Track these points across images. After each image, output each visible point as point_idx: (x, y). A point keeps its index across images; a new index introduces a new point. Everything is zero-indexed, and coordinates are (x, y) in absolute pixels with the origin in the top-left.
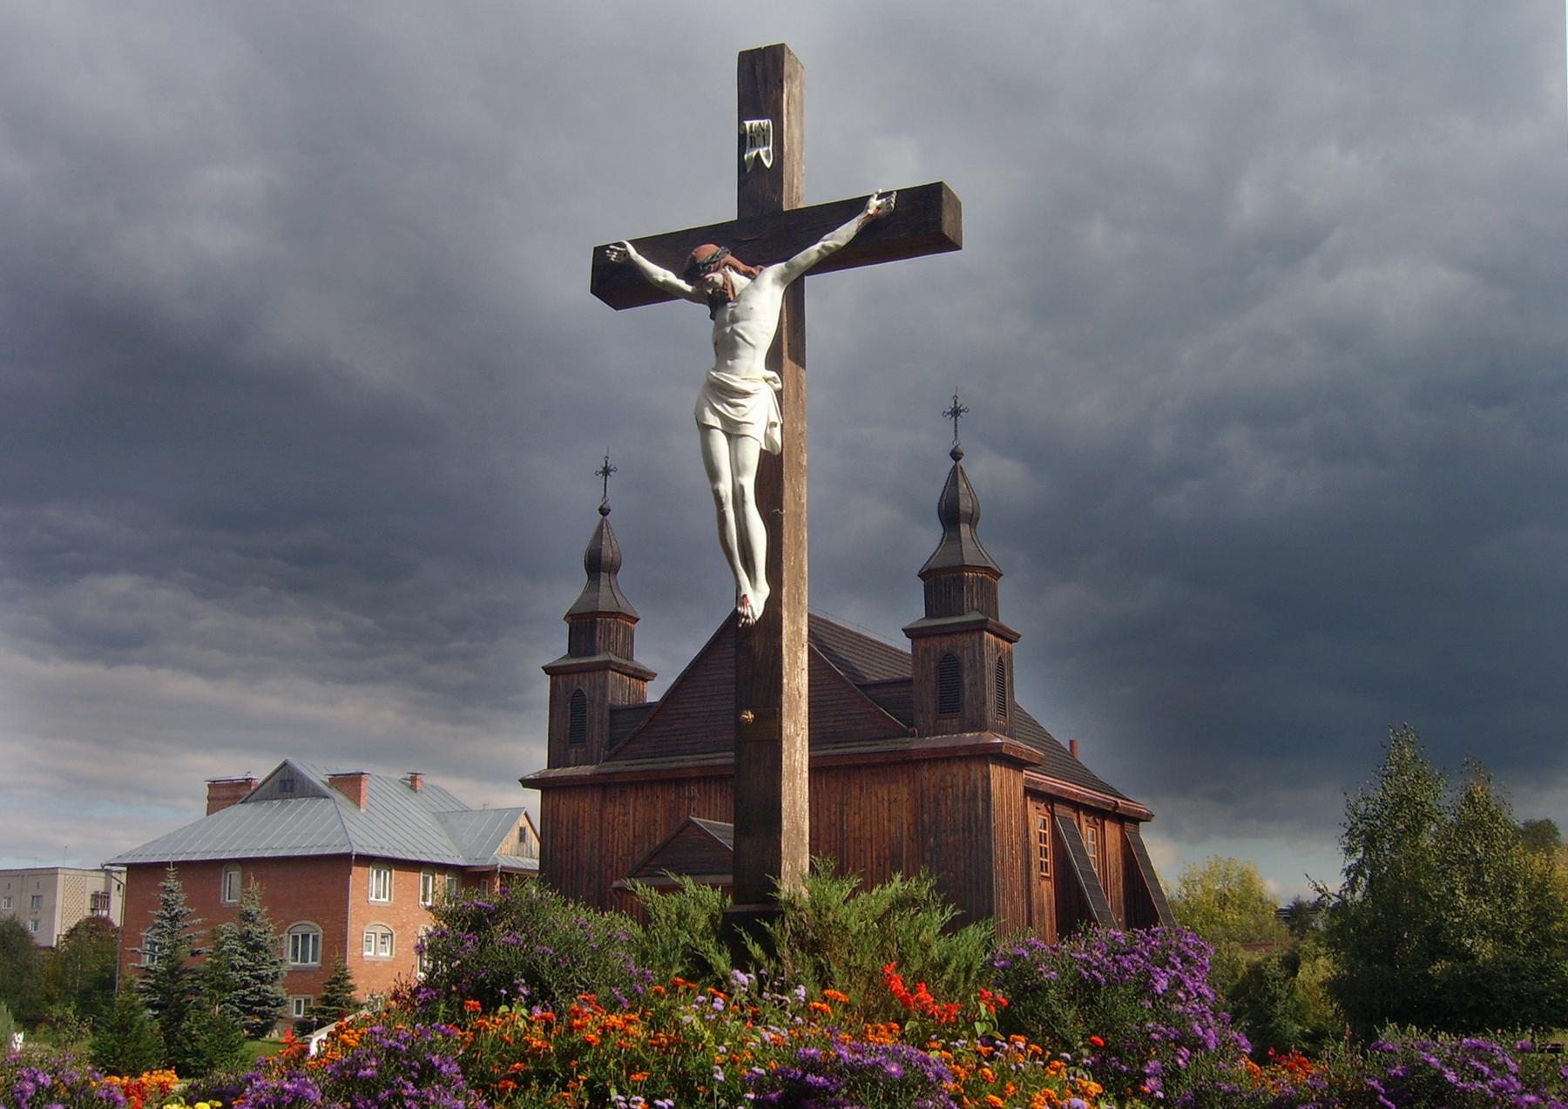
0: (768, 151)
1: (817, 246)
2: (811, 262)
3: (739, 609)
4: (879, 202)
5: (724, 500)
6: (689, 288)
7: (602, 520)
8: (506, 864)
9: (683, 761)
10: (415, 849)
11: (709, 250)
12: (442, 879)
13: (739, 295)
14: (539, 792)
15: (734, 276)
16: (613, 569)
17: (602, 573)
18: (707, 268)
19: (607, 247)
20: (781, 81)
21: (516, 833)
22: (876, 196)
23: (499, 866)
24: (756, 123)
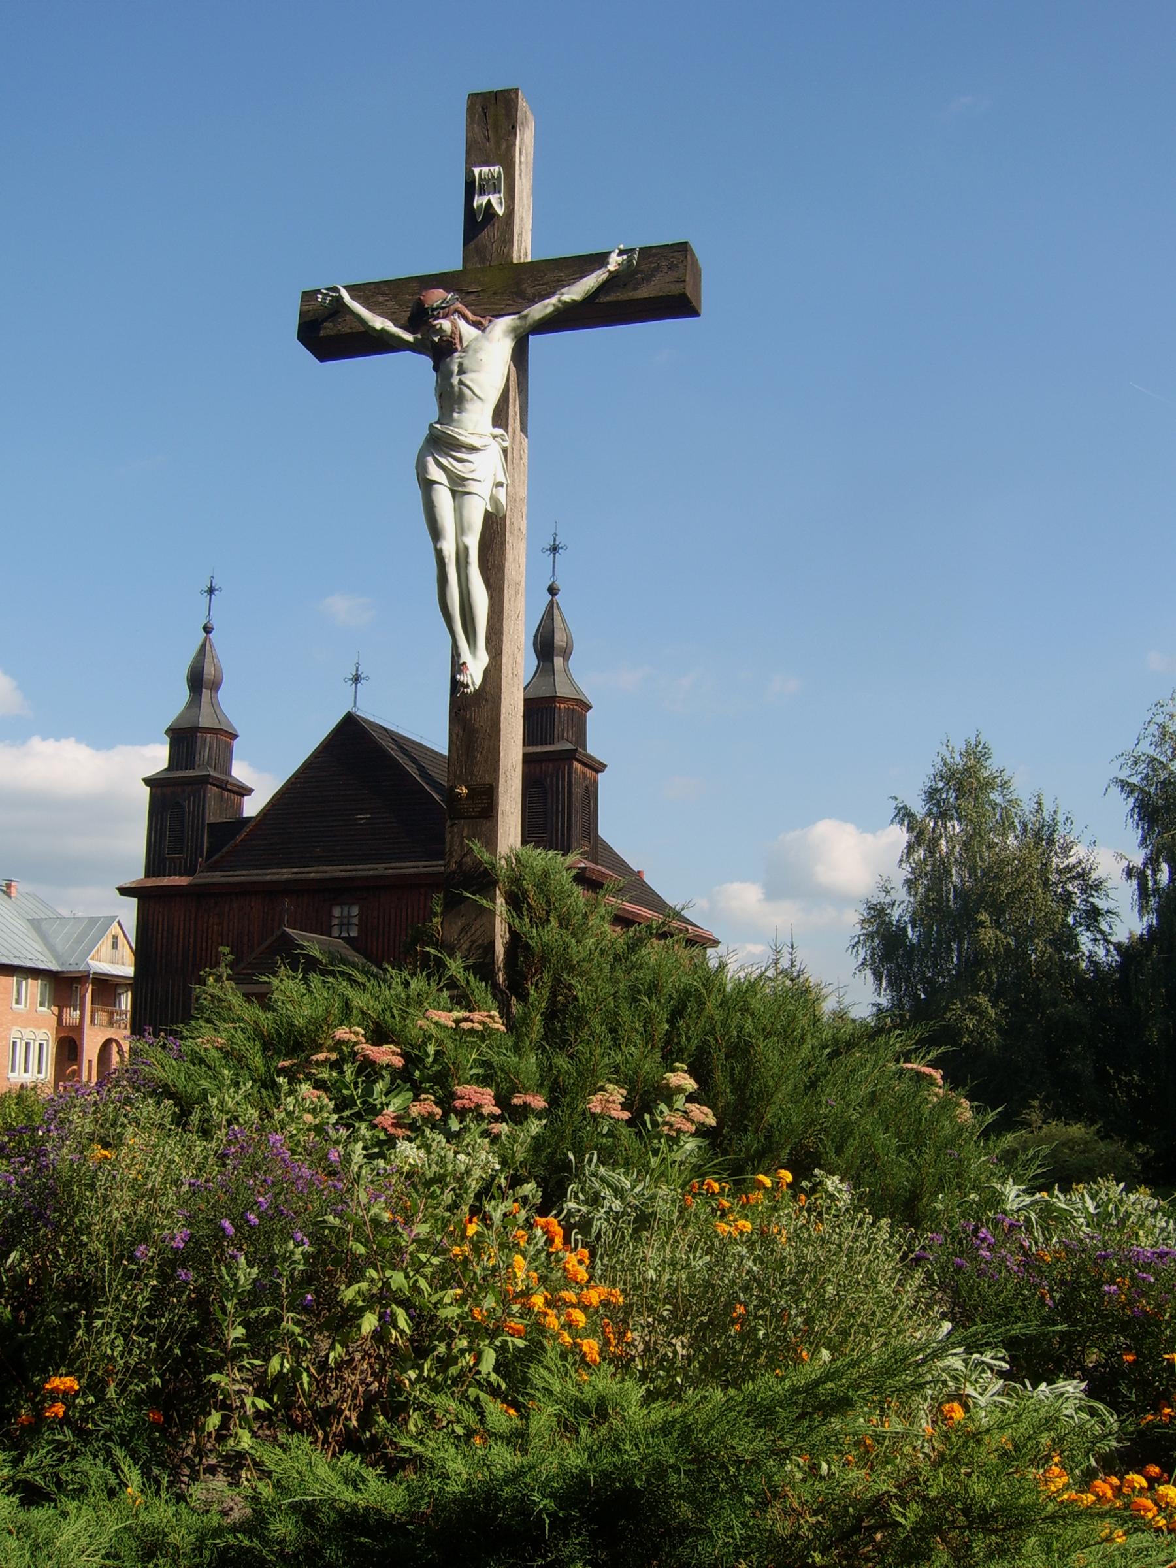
0: (500, 198)
1: (554, 300)
2: (589, 291)
3: (458, 676)
4: (620, 259)
5: (446, 560)
6: (409, 337)
7: (206, 638)
8: (99, 971)
9: (277, 874)
10: (10, 954)
11: (437, 297)
12: (33, 987)
13: (467, 346)
14: (135, 900)
15: (463, 325)
16: (215, 686)
17: (204, 690)
18: (435, 313)
19: (319, 291)
20: (514, 127)
21: (110, 941)
22: (617, 251)
23: (92, 972)
24: (485, 170)
